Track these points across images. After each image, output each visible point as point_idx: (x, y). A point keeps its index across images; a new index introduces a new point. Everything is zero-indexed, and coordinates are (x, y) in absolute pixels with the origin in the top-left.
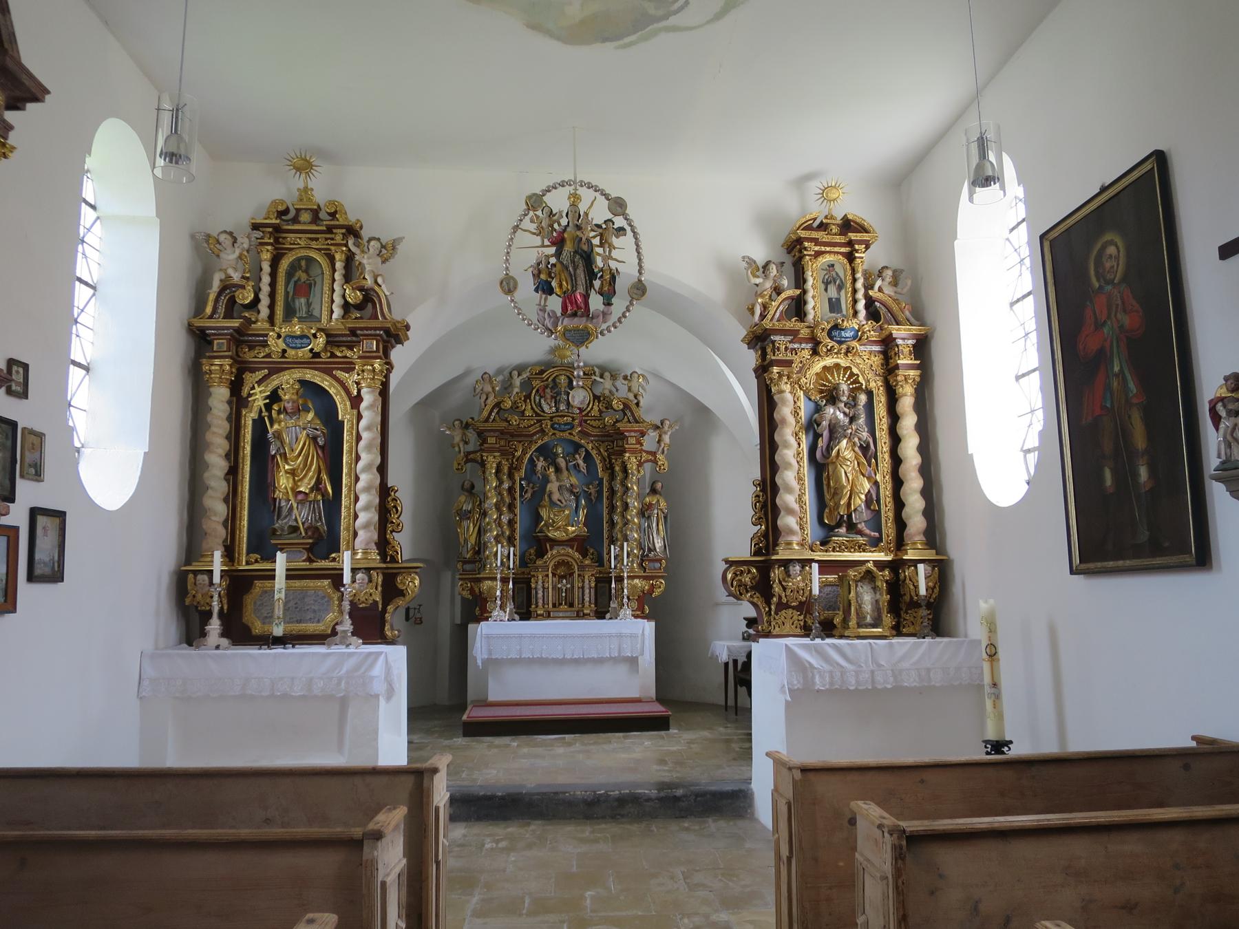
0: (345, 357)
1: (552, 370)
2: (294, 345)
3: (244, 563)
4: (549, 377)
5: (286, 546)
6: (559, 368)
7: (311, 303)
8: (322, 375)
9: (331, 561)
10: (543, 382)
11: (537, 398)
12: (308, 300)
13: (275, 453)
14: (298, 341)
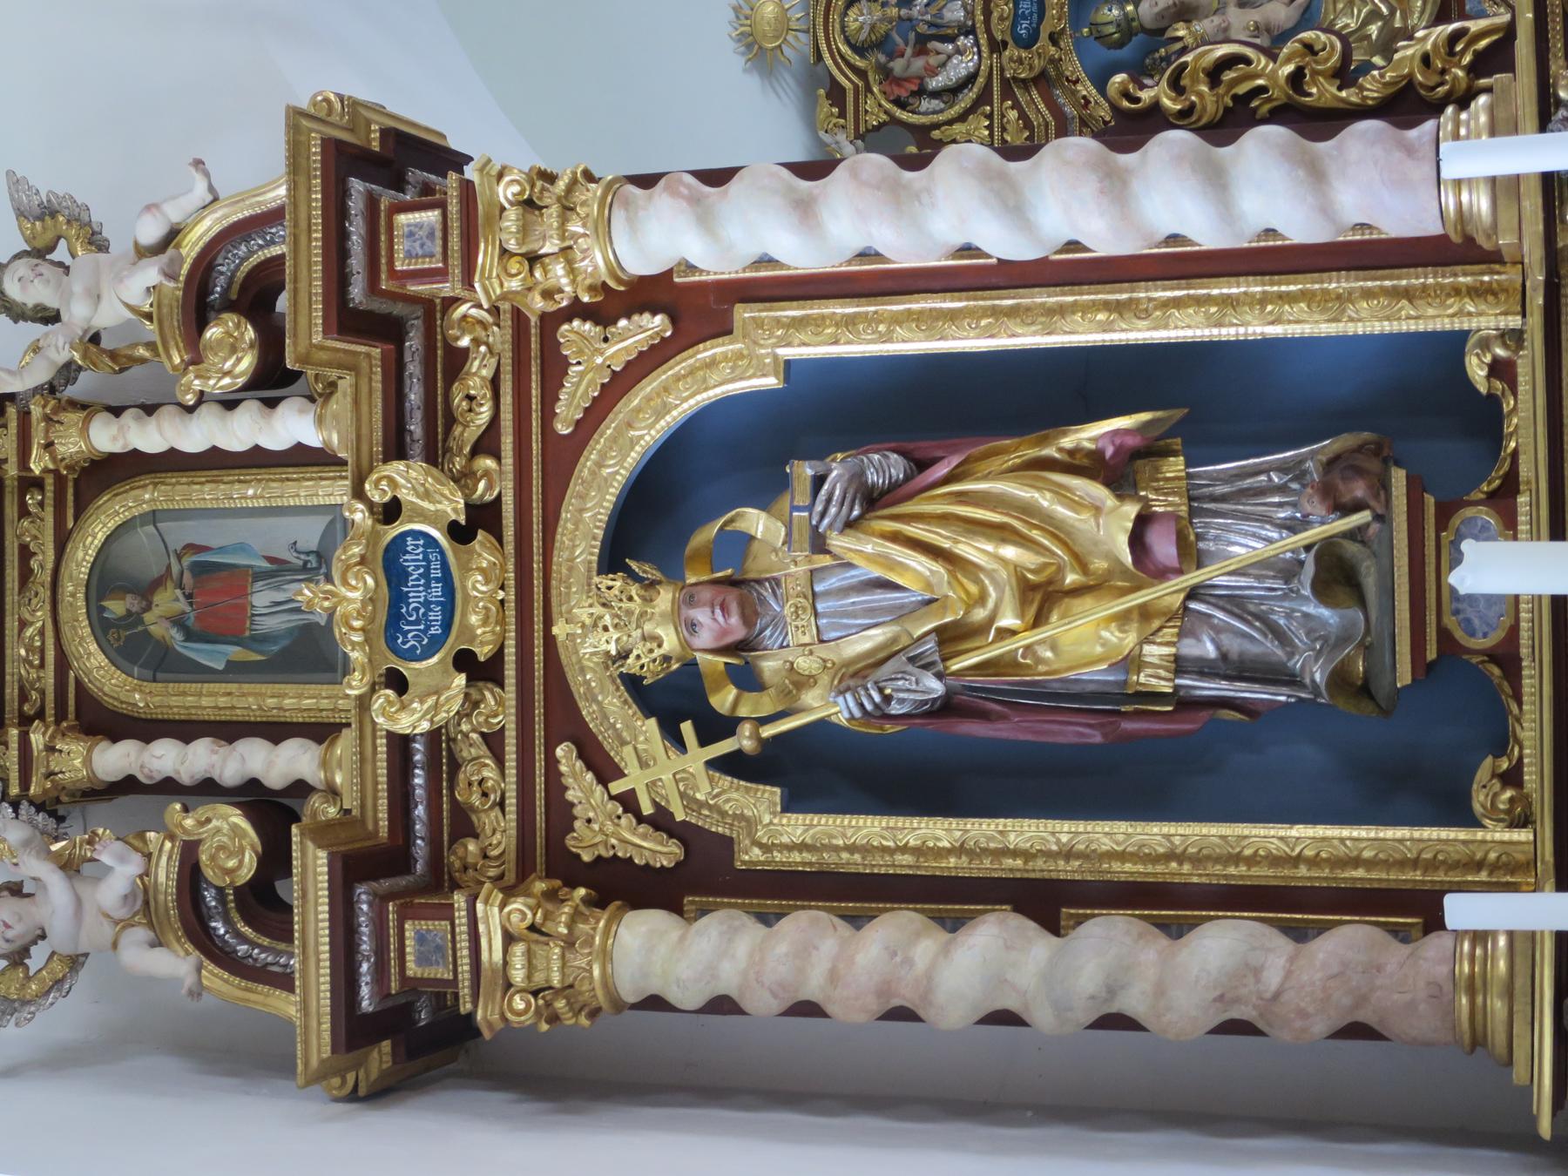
1: (829, 62)
2: (436, 615)
3: (1524, 835)
4: (842, 57)
5: (1431, 618)
6: (821, 34)
7: (271, 560)
9: (1513, 388)
10: (869, 89)
11: (926, 104)
12: (260, 575)
13: (940, 676)
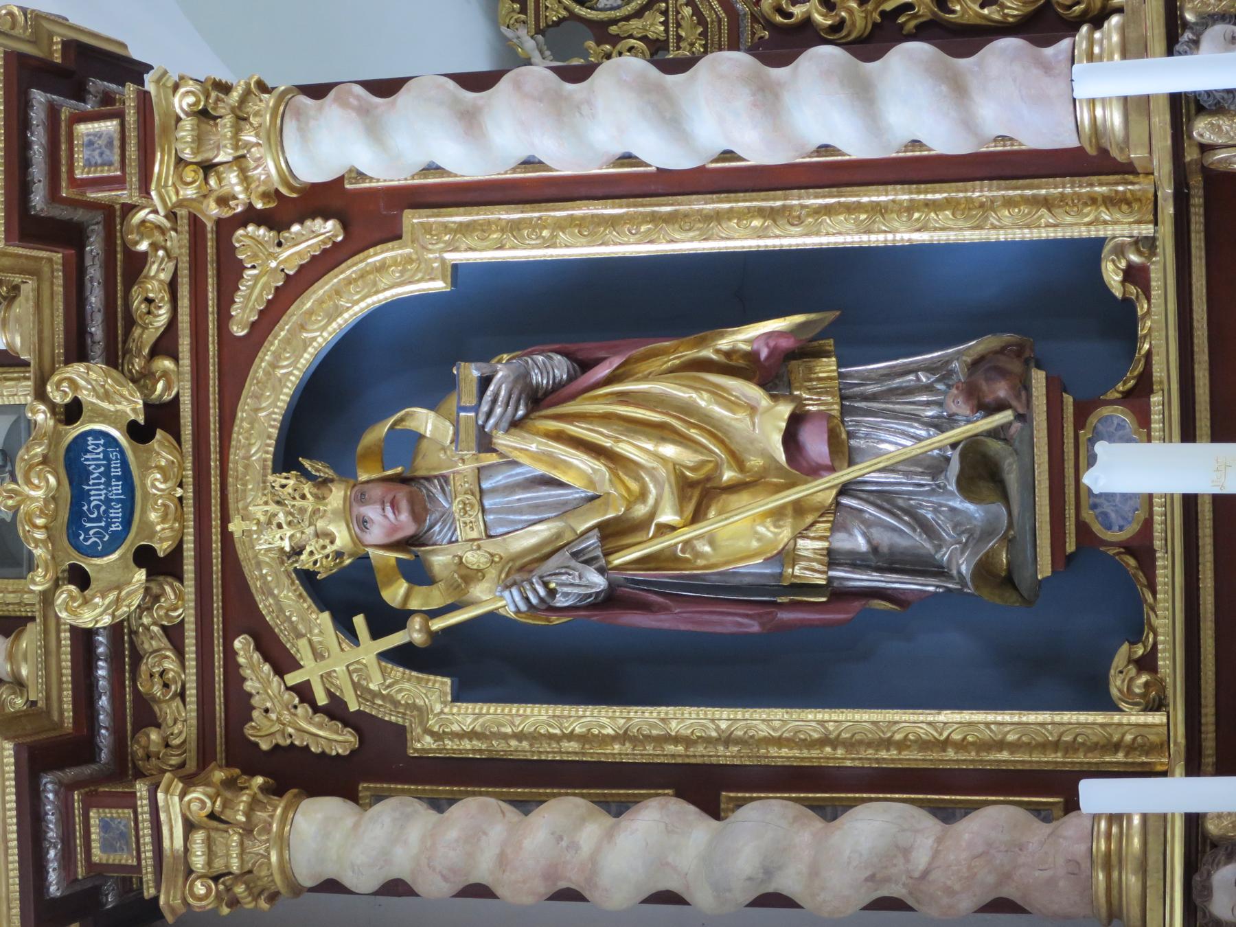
0: (173, 286)
2: (116, 512)
3: (1158, 718)
5: (1070, 512)
8: (250, 387)
13: (601, 571)
14: (97, 495)
